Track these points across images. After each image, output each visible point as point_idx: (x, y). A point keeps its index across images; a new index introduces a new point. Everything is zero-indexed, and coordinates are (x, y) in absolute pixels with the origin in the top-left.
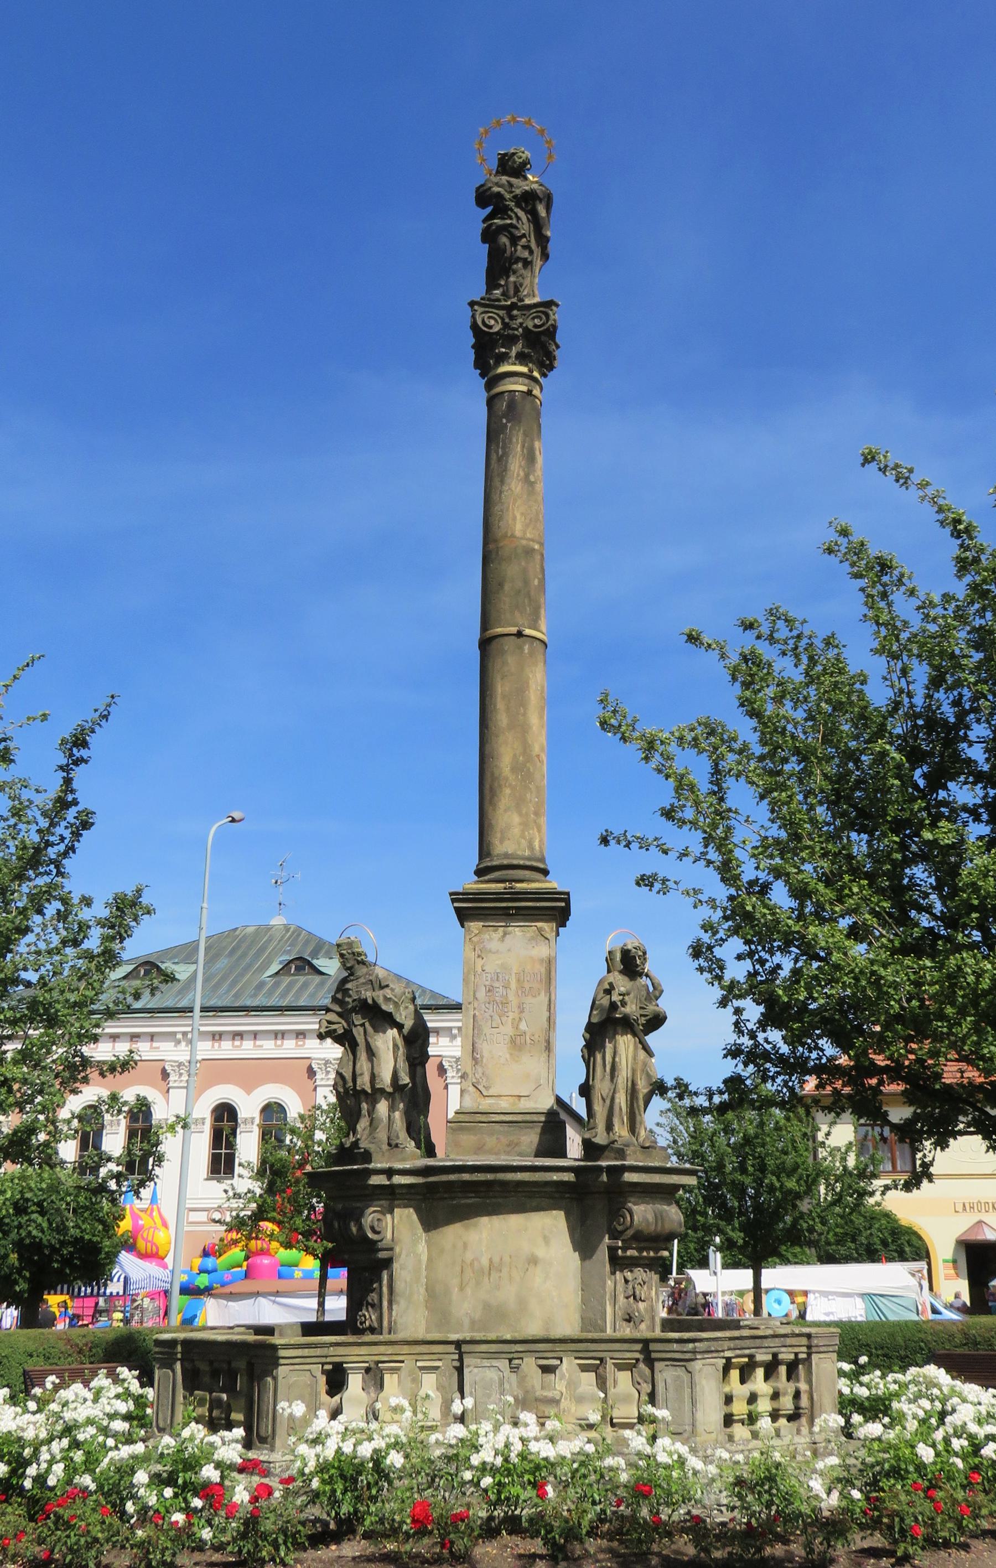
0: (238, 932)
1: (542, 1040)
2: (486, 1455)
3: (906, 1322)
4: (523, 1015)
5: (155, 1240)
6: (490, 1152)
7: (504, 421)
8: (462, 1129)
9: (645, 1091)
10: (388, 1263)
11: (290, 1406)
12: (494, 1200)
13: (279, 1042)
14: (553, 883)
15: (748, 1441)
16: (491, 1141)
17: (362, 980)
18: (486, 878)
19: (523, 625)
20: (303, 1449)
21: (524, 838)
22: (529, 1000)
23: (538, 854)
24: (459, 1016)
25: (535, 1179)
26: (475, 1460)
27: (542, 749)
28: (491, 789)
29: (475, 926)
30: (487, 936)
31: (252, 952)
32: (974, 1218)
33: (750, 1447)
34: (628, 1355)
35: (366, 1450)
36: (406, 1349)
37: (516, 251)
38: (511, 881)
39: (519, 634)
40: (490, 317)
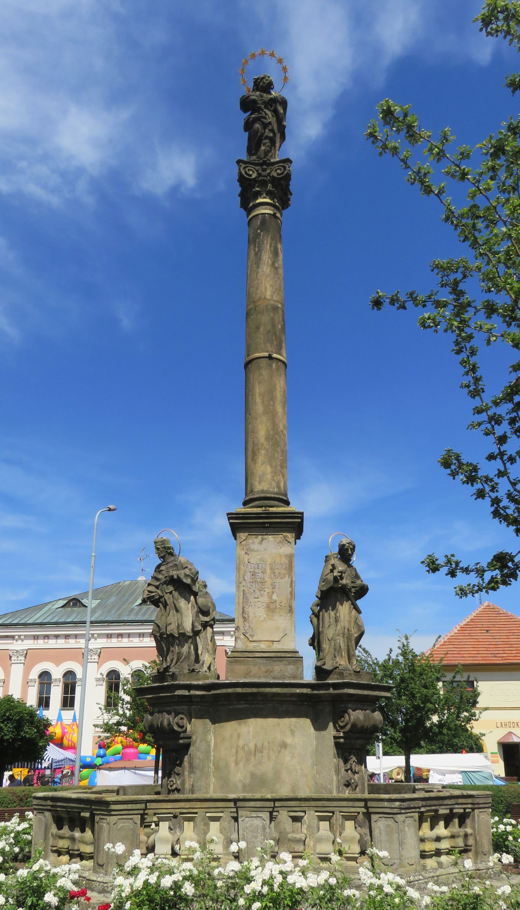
0: (121, 584)
1: (287, 605)
2: (256, 886)
3: (487, 785)
4: (275, 590)
5: (73, 740)
6: (254, 676)
7: (259, 231)
8: (236, 662)
9: (356, 635)
10: (186, 747)
11: (114, 847)
12: (257, 706)
13: (141, 639)
14: (293, 507)
15: (436, 869)
16: (255, 670)
17: (170, 565)
18: (251, 505)
19: (272, 351)
20: (120, 880)
21: (274, 480)
22: (278, 580)
23: (283, 491)
24: (233, 625)
25: (285, 692)
26: (248, 889)
27: (284, 427)
28: (253, 452)
29: (242, 536)
30: (251, 541)
31: (127, 594)
32: (507, 730)
33: (438, 873)
34: (352, 810)
35: (167, 882)
36: (198, 804)
37: (265, 132)
38: (266, 507)
39: (270, 357)
40: (249, 170)
